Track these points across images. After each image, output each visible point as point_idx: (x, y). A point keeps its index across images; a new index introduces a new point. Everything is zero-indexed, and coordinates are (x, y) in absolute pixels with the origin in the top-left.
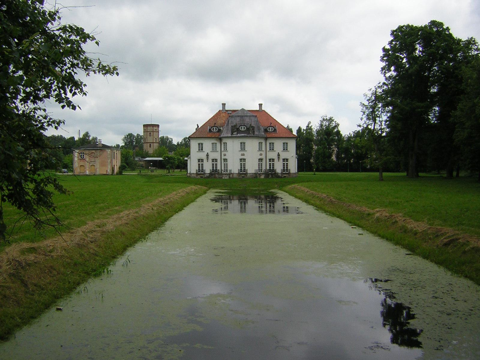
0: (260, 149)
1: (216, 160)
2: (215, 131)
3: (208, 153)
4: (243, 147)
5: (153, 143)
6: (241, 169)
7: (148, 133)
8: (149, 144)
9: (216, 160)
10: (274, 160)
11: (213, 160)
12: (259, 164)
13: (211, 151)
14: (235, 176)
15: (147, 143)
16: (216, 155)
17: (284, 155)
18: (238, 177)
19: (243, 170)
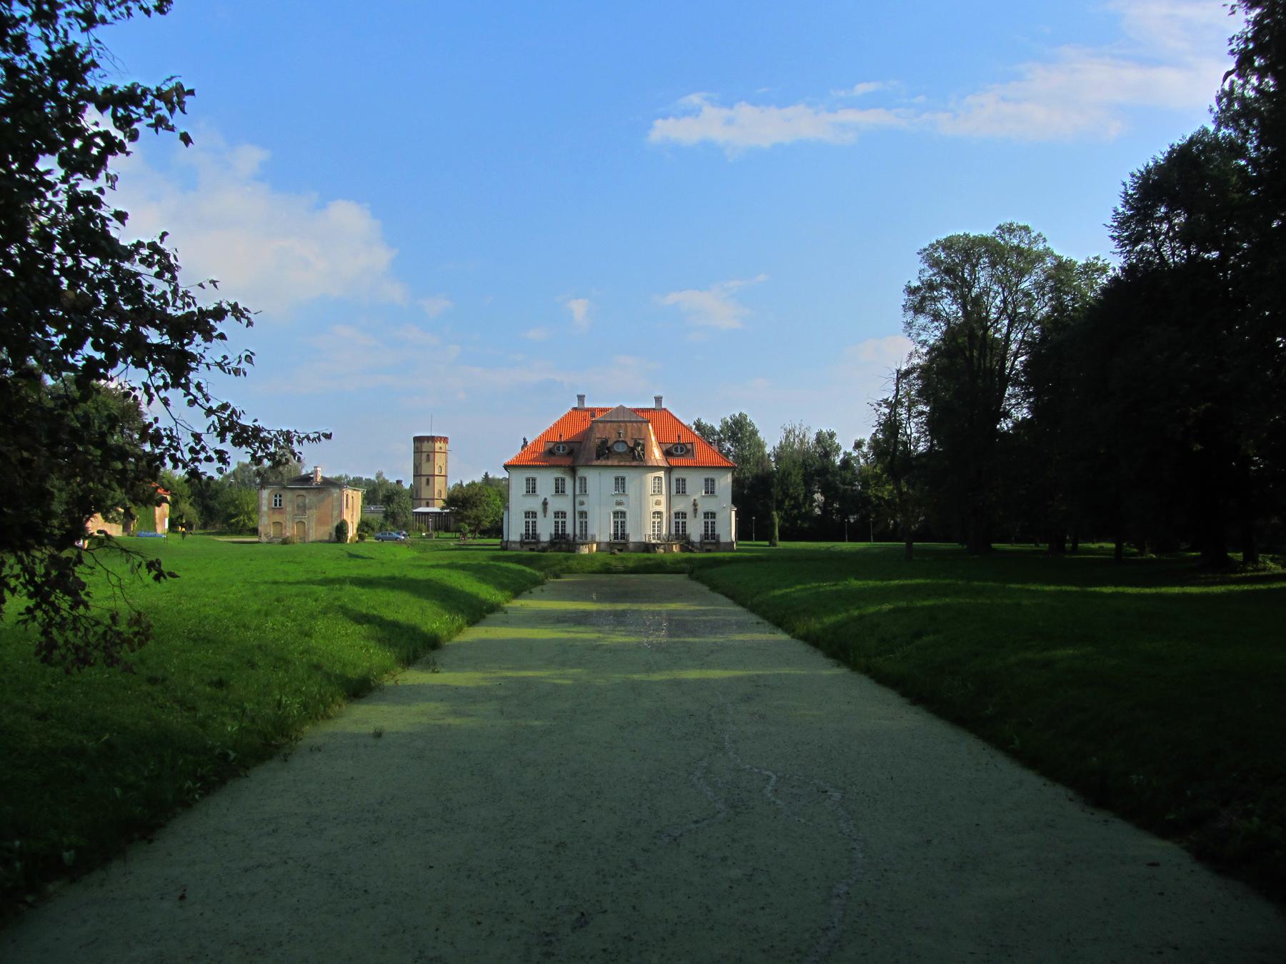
1: (564, 514)
2: (561, 451)
3: (545, 499)
9: (564, 514)
16: (564, 504)
17: (707, 505)
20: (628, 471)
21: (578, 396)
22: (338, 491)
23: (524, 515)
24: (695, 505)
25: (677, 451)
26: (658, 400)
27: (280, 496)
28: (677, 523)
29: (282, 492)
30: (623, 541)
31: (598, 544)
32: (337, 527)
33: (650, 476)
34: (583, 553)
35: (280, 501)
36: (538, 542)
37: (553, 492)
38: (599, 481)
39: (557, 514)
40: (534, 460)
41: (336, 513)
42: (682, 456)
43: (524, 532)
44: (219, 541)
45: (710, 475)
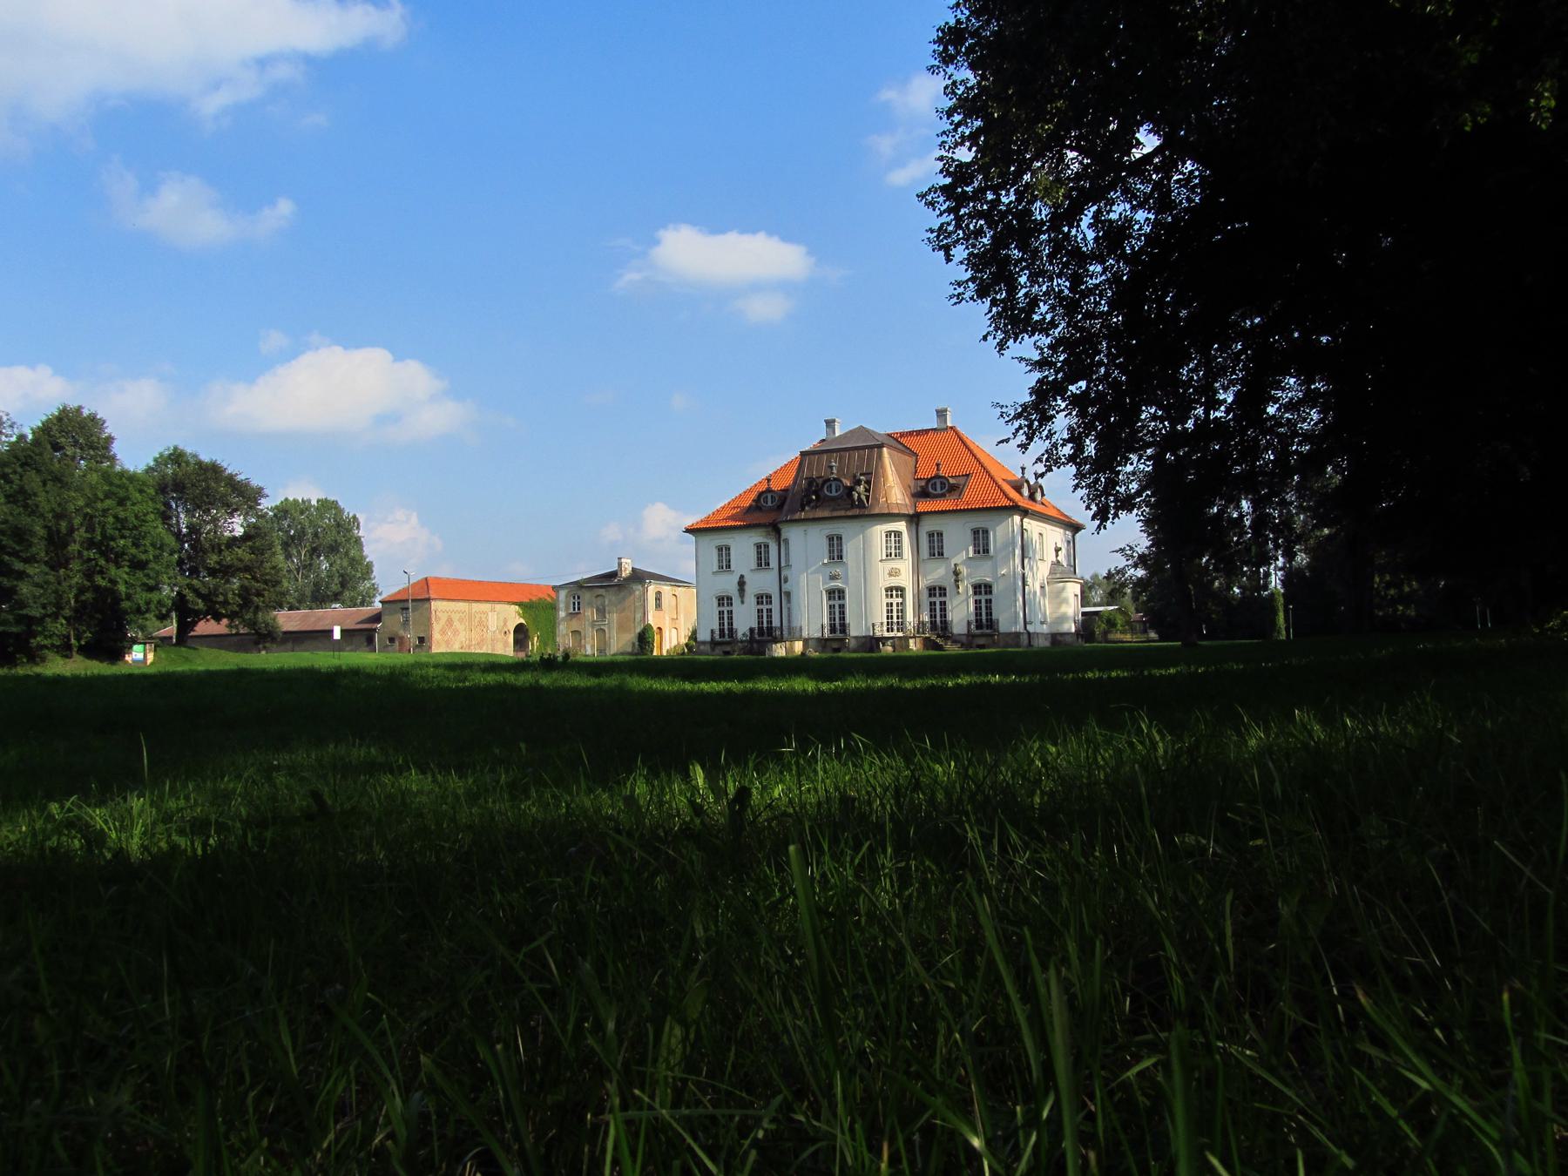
2: (769, 504)
3: (742, 577)
6: (933, 619)
10: (990, 587)
11: (977, 588)
12: (721, 613)
13: (753, 568)
19: (984, 621)
20: (845, 525)
21: (826, 421)
22: (640, 587)
23: (715, 602)
24: (956, 573)
25: (936, 490)
26: (941, 414)
27: (579, 598)
28: (932, 604)
29: (580, 593)
31: (806, 642)
32: (639, 634)
33: (879, 531)
34: (442, 649)
35: (579, 603)
37: (753, 565)
38: (805, 541)
40: (733, 518)
41: (638, 616)
42: (943, 495)
43: (757, 626)
44: (968, 673)
45: (979, 522)
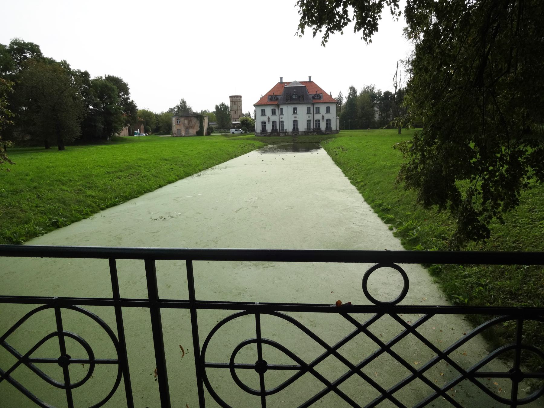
0: (309, 112)
1: (275, 122)
3: (323, 115)
4: (295, 111)
5: (238, 110)
7: (234, 102)
8: (234, 111)
9: (275, 122)
14: (290, 134)
15: (233, 110)
16: (275, 118)
17: (327, 117)
18: (292, 134)
30: (297, 131)
36: (267, 133)
39: (273, 122)
45: (263, 108)
